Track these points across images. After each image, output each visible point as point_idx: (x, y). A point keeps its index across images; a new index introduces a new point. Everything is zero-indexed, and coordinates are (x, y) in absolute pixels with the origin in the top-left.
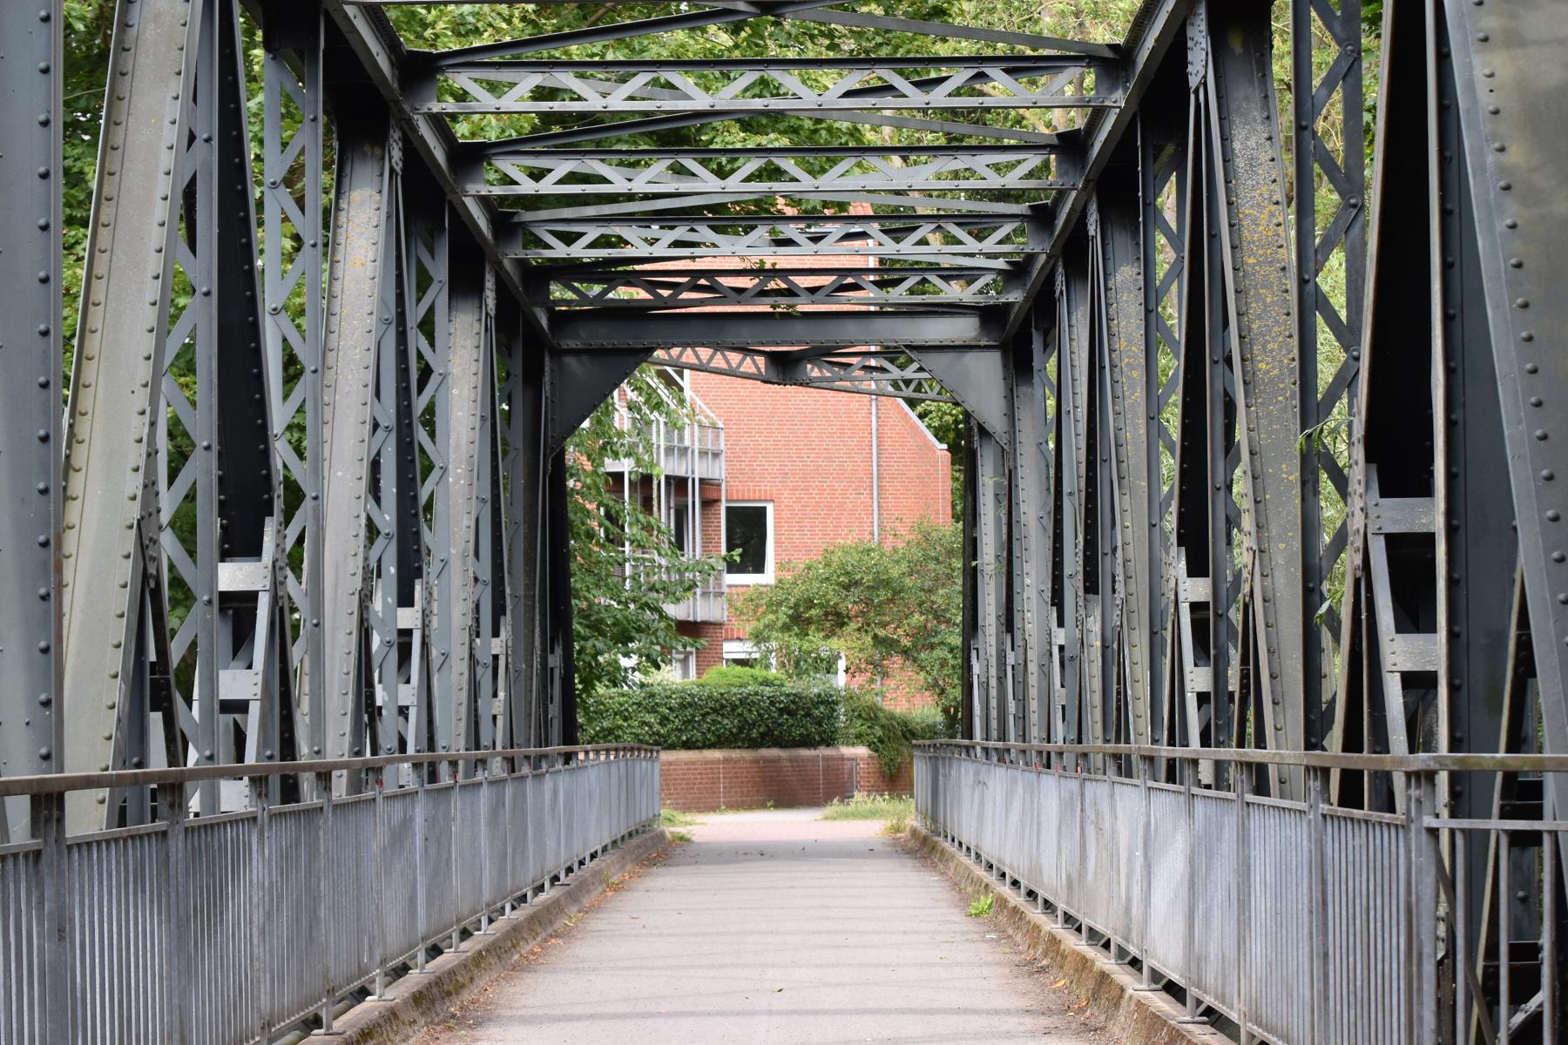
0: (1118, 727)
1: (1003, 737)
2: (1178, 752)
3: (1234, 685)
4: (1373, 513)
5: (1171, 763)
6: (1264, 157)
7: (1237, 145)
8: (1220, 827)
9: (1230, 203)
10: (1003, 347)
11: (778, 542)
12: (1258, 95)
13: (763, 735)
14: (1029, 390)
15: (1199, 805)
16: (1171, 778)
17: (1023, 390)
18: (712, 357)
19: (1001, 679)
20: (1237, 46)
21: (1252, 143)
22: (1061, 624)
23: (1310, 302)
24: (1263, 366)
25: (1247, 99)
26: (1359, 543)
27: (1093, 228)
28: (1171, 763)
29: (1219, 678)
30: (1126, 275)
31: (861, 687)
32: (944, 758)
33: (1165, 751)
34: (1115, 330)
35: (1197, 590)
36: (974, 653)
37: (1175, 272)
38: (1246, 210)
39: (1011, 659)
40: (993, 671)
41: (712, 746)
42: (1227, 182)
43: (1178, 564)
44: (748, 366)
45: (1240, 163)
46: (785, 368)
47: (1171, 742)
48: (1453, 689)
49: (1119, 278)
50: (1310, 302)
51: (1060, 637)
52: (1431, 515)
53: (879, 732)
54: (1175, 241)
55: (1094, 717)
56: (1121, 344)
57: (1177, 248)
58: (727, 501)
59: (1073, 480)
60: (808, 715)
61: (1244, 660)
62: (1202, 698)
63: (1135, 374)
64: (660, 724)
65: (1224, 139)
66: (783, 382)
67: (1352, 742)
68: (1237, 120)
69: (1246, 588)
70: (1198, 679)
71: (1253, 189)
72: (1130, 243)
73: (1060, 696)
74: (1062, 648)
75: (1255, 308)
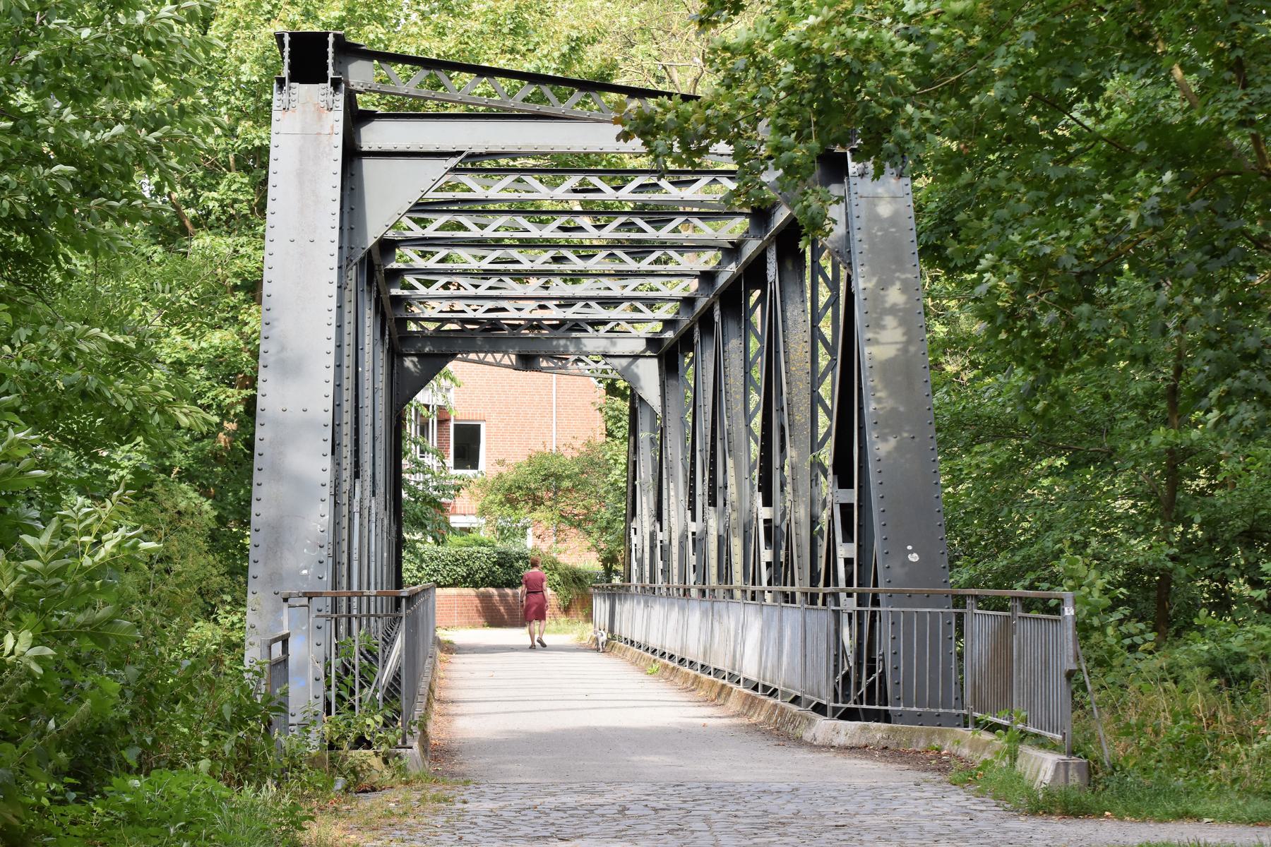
0: (725, 573)
1: (652, 579)
2: (757, 588)
3: (782, 559)
4: (835, 495)
5: (754, 592)
6: (801, 320)
7: (788, 314)
8: (772, 616)
9: (784, 342)
10: (659, 357)
11: (488, 449)
12: (798, 291)
13: (482, 579)
14: (675, 382)
15: (765, 608)
16: (753, 599)
17: (672, 382)
18: (485, 357)
19: (652, 548)
20: (789, 266)
21: (795, 313)
22: (694, 519)
23: (816, 400)
24: (797, 418)
25: (794, 292)
26: (830, 506)
27: (717, 317)
28: (754, 592)
29: (776, 555)
30: (734, 344)
31: (550, 547)
32: (620, 594)
33: (751, 587)
34: (728, 373)
35: (765, 513)
36: (632, 531)
37: (759, 353)
38: (791, 345)
39: (660, 536)
40: (647, 543)
41: (450, 586)
42: (784, 331)
43: (759, 498)
44: (506, 361)
45: (790, 323)
46: (527, 362)
47: (754, 584)
48: (859, 565)
49: (730, 346)
50: (816, 400)
51: (693, 527)
52: (852, 496)
53: (557, 578)
54: (760, 339)
55: (713, 571)
56: (731, 381)
57: (761, 341)
58: (455, 420)
59: (702, 443)
60: (511, 566)
61: (787, 549)
62: (768, 564)
63: (738, 397)
64: (418, 570)
65: (782, 311)
66: (526, 369)
67: (827, 584)
68: (789, 302)
69: (788, 517)
70: (766, 555)
71: (795, 335)
72: (736, 328)
73: (692, 560)
74: (694, 534)
75: (795, 391)
